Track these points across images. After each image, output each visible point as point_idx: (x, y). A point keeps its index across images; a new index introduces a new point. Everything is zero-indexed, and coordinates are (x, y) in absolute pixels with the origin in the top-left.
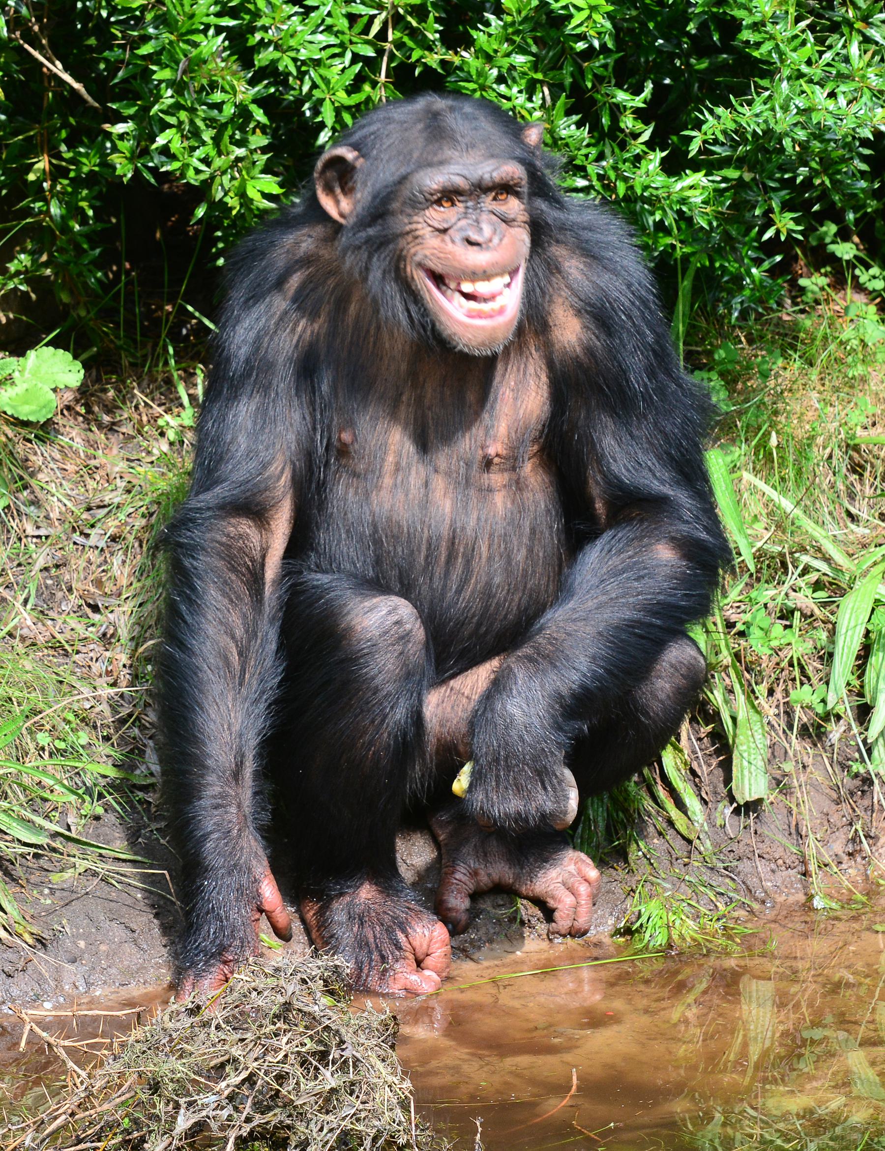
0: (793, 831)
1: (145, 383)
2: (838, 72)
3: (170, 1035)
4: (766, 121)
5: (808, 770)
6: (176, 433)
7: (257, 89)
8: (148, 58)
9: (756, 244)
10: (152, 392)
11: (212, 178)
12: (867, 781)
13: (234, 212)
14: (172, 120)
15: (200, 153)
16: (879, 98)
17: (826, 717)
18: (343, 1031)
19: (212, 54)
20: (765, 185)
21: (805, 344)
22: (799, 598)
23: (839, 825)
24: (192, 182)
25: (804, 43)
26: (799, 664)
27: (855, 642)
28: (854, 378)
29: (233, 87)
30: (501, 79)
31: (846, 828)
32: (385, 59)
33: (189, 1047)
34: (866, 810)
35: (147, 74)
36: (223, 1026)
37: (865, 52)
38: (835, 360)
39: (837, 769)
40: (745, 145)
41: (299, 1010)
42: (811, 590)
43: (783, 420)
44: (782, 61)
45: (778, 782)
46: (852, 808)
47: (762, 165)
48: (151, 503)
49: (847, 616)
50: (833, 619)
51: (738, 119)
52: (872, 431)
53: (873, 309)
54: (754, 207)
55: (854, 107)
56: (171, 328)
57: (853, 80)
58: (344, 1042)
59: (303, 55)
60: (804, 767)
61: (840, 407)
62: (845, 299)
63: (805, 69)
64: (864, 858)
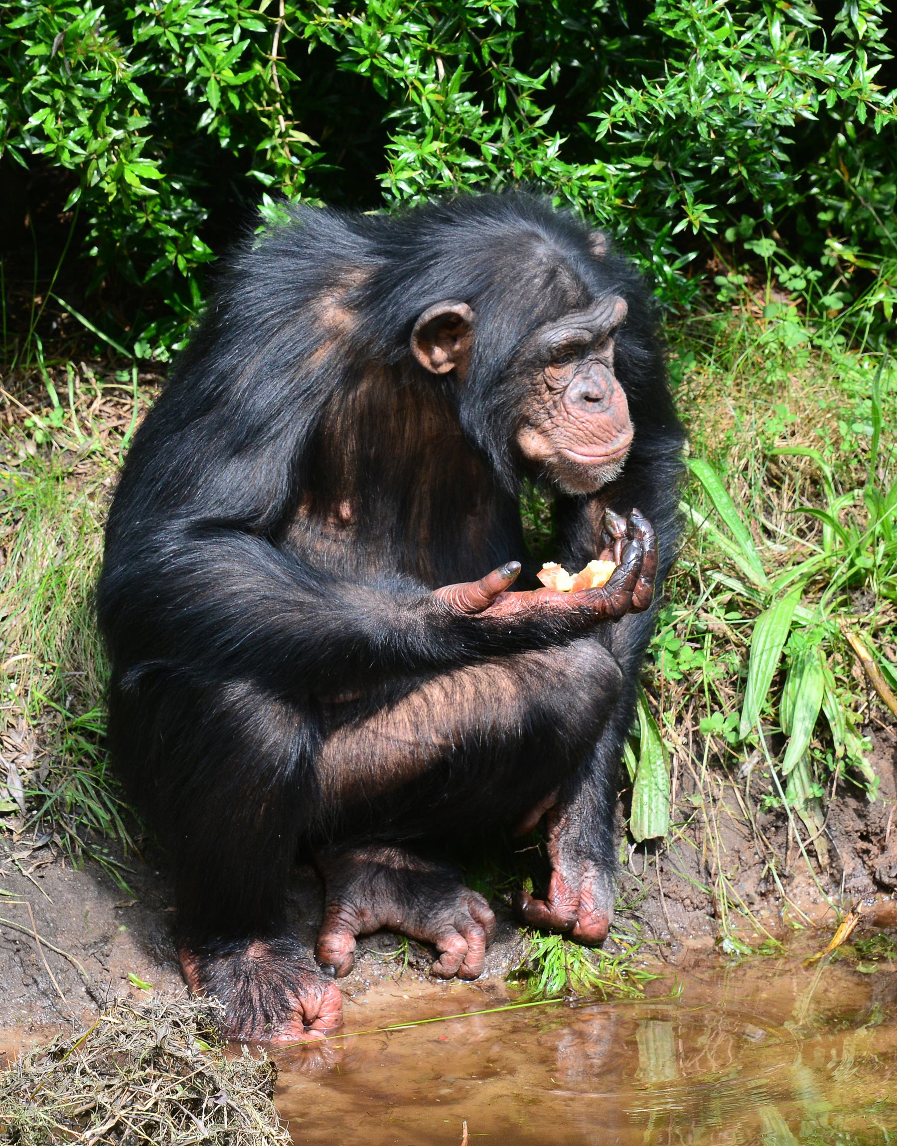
0: (702, 869)
1: (11, 381)
2: (758, 54)
3: (32, 1081)
4: (680, 105)
5: (719, 804)
6: (45, 435)
7: (136, 67)
8: (21, 32)
9: (669, 239)
10: (18, 390)
11: (87, 163)
12: (781, 816)
13: (111, 199)
14: (46, 99)
15: (75, 134)
16: (801, 84)
17: (739, 747)
18: (217, 1077)
19: (90, 28)
20: (677, 175)
21: (721, 347)
22: (712, 620)
23: (751, 862)
24: (67, 165)
25: (721, 23)
26: (710, 690)
27: (770, 667)
28: (772, 384)
29: (112, 65)
30: (392, 48)
31: (758, 866)
32: (277, 35)
33: (52, 1093)
34: (780, 847)
35: (18, 50)
36: (89, 1071)
37: (787, 34)
38: (753, 364)
39: (750, 803)
40: (657, 131)
41: (171, 1055)
42: (723, 611)
43: (696, 428)
44: (698, 41)
45: (687, 817)
46: (766, 846)
47: (675, 153)
48: (17, 508)
49: (762, 639)
50: (746, 641)
51: (650, 101)
52: (791, 441)
53: (793, 310)
54: (665, 199)
55: (775, 92)
56: (40, 321)
57: (775, 63)
58: (218, 1090)
59: (187, 30)
60: (714, 800)
61: (757, 415)
62: (763, 299)
63: (723, 50)
64: (777, 899)
